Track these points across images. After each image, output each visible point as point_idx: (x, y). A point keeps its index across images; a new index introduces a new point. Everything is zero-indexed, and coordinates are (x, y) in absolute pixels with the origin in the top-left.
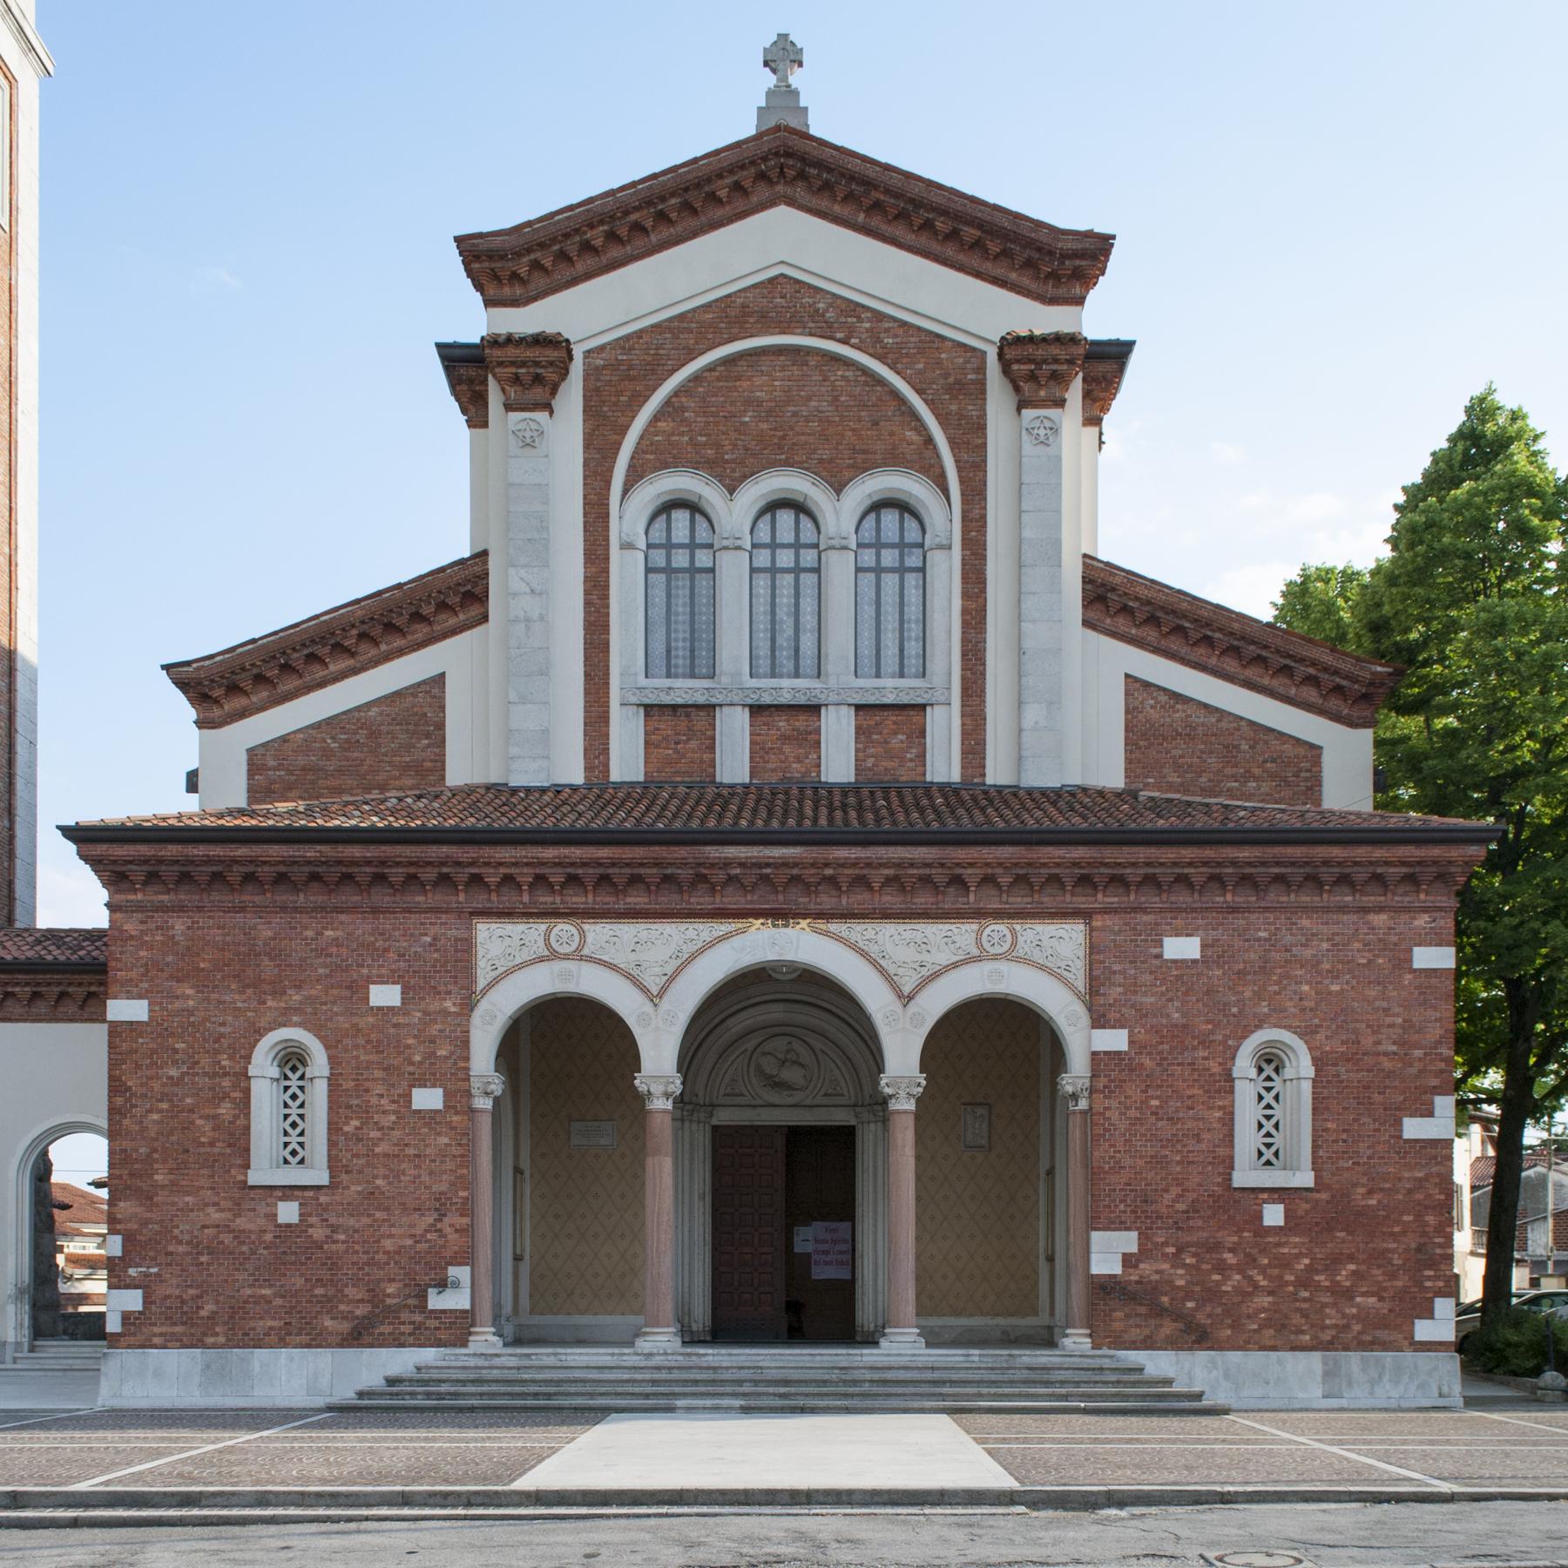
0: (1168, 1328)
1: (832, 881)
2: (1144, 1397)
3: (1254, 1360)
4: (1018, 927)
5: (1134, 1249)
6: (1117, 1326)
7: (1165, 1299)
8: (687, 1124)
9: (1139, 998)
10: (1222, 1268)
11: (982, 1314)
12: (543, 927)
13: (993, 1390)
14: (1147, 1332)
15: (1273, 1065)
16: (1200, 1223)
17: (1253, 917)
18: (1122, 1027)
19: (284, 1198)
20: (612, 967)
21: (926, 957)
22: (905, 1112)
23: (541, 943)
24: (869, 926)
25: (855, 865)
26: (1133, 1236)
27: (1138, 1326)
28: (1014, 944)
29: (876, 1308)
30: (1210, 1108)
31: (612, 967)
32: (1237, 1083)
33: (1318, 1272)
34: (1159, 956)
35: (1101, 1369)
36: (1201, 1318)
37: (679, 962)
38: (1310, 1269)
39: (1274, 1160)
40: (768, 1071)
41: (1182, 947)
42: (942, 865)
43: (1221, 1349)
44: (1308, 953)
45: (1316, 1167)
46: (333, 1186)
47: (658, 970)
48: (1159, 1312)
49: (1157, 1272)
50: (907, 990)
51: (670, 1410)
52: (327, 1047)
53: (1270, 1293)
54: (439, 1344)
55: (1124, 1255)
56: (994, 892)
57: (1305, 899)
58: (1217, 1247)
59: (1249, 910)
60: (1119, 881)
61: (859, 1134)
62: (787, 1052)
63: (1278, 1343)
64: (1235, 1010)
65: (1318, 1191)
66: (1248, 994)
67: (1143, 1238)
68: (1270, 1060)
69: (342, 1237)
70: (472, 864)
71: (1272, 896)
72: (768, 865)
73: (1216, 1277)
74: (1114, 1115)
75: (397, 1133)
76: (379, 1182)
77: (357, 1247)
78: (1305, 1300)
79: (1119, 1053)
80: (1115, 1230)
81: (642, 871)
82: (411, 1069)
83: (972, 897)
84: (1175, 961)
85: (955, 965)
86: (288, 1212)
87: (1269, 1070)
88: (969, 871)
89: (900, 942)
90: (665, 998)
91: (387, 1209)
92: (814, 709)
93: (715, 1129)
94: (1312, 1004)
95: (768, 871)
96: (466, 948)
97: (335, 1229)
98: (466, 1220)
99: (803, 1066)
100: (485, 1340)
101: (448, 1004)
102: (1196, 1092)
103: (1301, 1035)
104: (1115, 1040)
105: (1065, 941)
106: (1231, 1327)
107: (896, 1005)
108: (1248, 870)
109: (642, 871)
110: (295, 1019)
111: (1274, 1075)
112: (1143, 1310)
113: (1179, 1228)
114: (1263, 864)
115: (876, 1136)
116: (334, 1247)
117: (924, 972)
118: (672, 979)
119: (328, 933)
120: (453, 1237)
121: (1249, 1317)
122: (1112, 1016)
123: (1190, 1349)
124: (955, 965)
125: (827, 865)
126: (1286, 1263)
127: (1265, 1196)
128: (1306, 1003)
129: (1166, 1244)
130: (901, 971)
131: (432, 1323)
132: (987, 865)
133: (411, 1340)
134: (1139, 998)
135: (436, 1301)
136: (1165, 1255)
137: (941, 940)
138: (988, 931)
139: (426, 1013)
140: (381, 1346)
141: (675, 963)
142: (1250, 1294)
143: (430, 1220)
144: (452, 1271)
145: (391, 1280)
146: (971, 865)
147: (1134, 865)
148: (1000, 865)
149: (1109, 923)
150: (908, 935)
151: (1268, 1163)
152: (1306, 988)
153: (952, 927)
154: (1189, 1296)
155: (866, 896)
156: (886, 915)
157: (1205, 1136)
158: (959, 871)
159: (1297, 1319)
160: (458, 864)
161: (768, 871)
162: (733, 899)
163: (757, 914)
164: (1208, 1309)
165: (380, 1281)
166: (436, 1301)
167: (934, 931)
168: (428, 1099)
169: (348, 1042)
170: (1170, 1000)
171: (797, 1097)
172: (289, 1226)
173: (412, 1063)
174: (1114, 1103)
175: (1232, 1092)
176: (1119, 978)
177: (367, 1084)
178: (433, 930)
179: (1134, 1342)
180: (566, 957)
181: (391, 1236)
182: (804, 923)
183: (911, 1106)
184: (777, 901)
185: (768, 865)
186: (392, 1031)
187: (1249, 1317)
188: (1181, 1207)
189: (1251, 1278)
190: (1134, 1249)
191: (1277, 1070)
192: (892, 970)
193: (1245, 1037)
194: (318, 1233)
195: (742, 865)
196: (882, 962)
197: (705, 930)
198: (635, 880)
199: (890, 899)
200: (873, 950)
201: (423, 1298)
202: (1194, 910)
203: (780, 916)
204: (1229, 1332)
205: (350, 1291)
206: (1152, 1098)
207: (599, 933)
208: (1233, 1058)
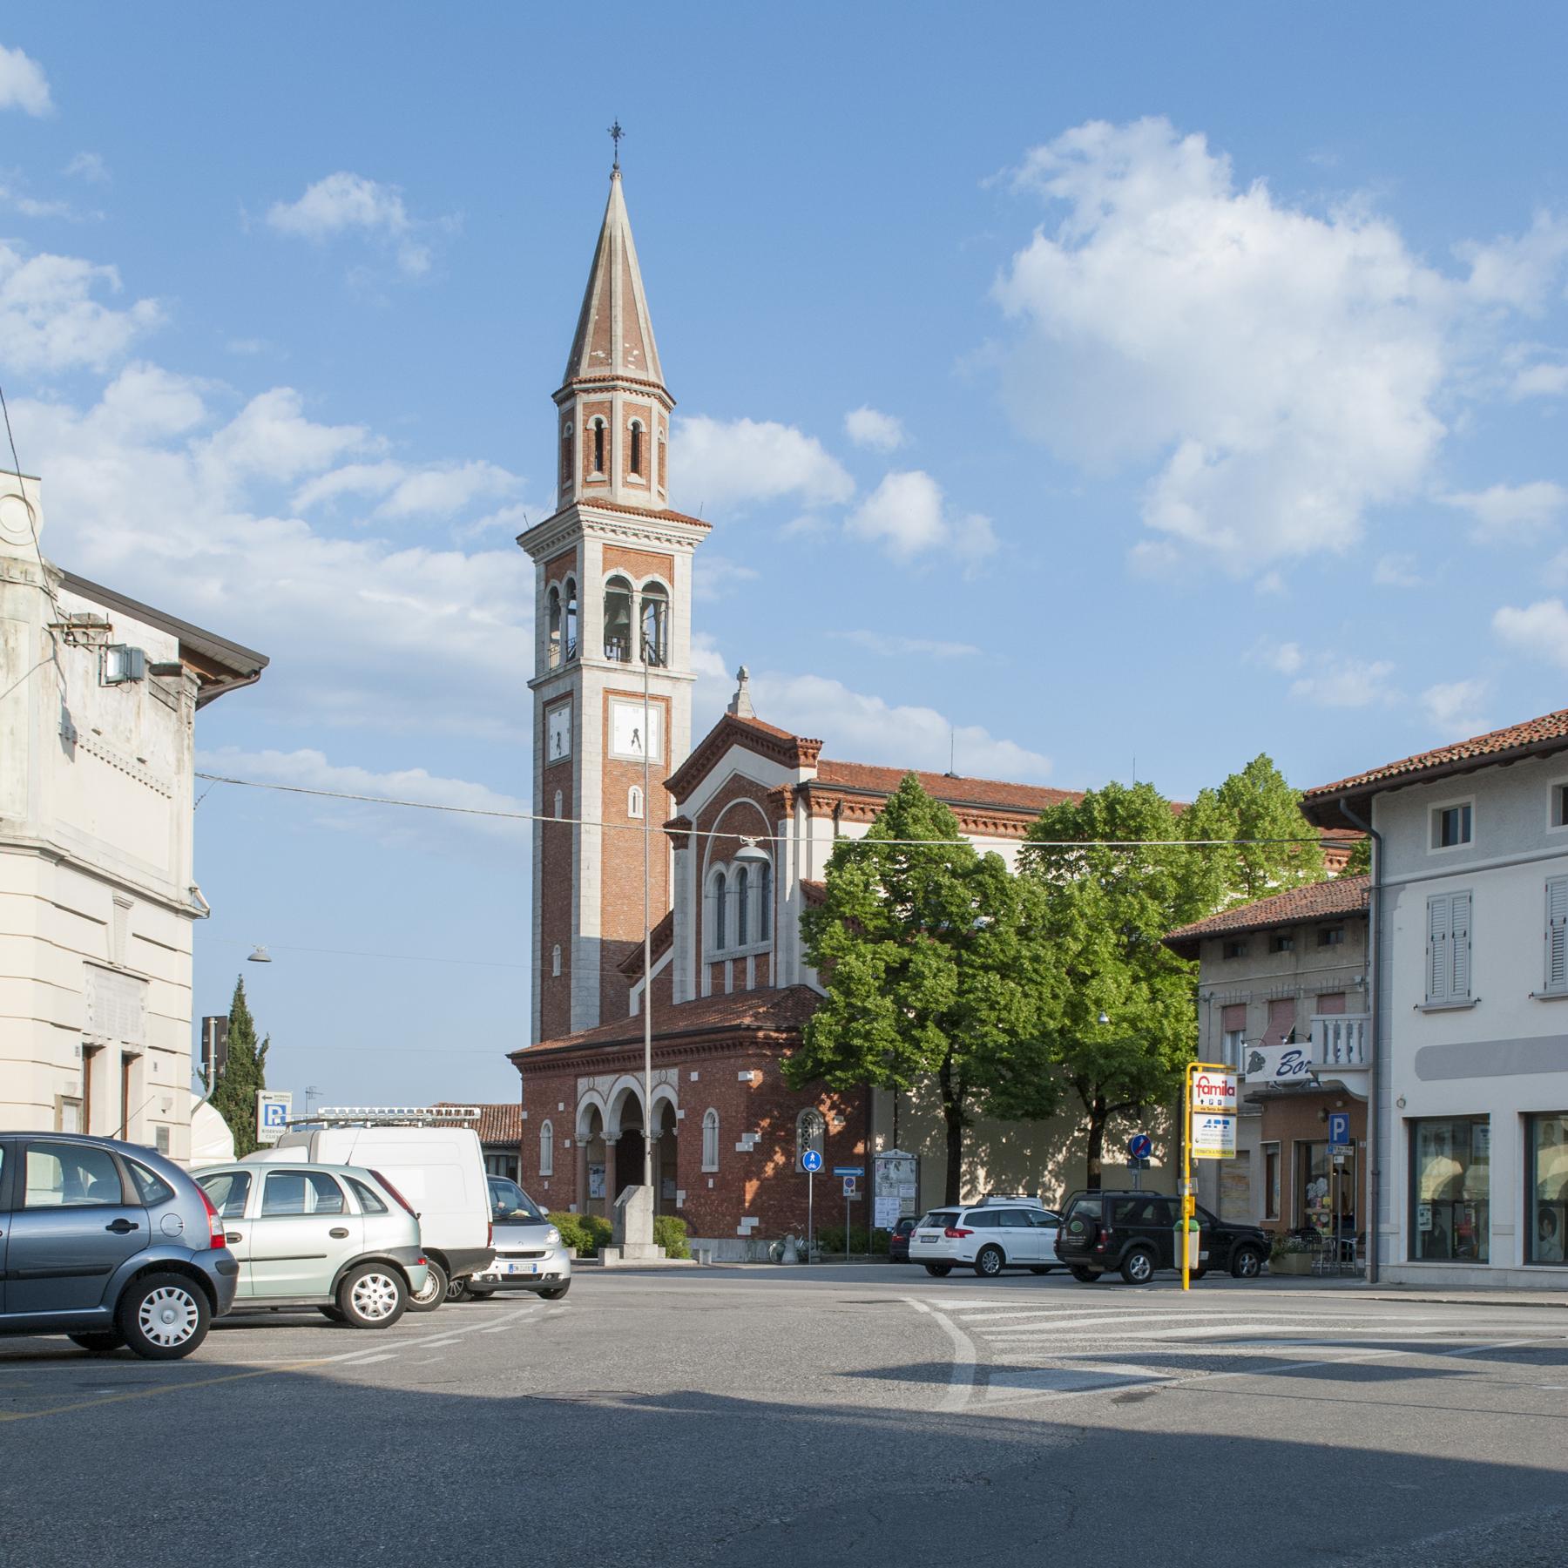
92: (744, 959)
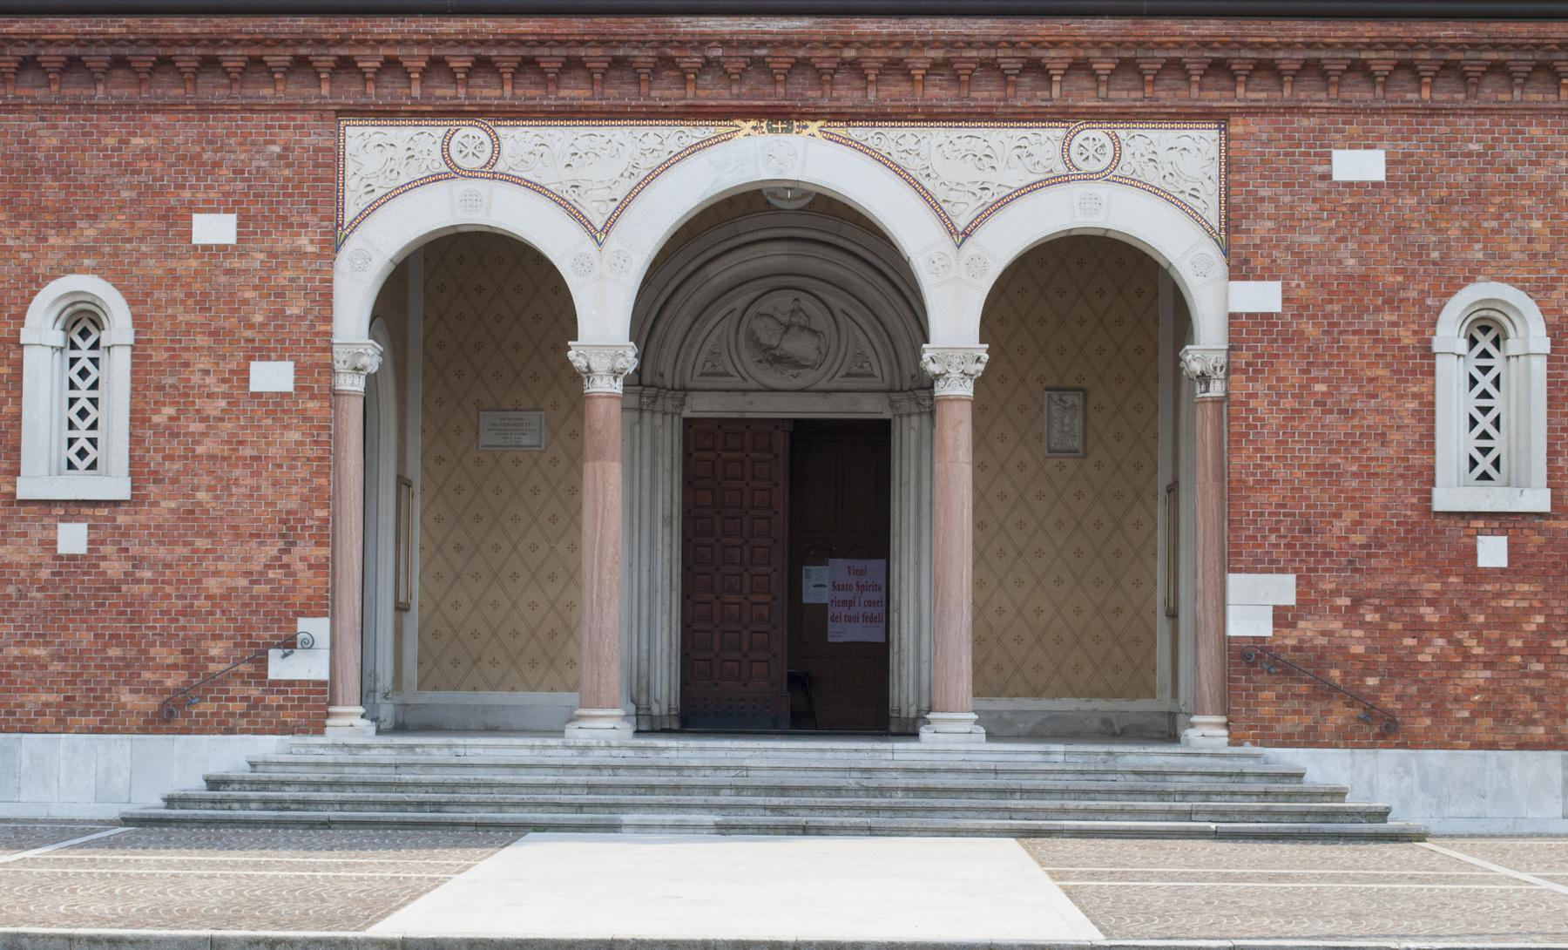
0: (1339, 715)
1: (855, 67)
2: (1303, 815)
3: (1464, 762)
4: (1122, 134)
5: (1290, 599)
6: (1265, 711)
7: (1335, 673)
8: (647, 416)
9: (1297, 237)
10: (1417, 628)
12: (441, 131)
13: (1083, 804)
14: (1309, 720)
15: (1492, 335)
16: (1386, 563)
17: (1460, 122)
18: (1273, 278)
19: (67, 518)
22: (959, 399)
23: (437, 155)
25: (887, 44)
26: (1290, 580)
27: (1298, 712)
28: (1117, 158)
30: (1400, 396)
32: (1439, 359)
33: (1556, 635)
34: (1326, 177)
35: (1242, 774)
36: (1388, 702)
38: (1546, 631)
39: (1492, 472)
41: (1359, 165)
42: (1013, 45)
43: (1416, 746)
44: (1539, 174)
45: (1554, 481)
46: (137, 500)
47: (605, 194)
48: (1327, 691)
49: (1324, 633)
51: (613, 828)
52: (132, 303)
53: (1489, 665)
54: (283, 729)
55: (1276, 608)
56: (1087, 83)
57: (1535, 97)
58: (1411, 597)
59: (1454, 112)
60: (1266, 69)
63: (1499, 738)
64: (1435, 255)
65: (1556, 518)
66: (1454, 233)
67: (1304, 583)
68: (1487, 329)
69: (148, 574)
70: (341, 42)
71: (1487, 92)
72: (762, 44)
73: (1409, 642)
74: (1262, 406)
75: (227, 426)
76: (201, 496)
77: (168, 589)
78: (1538, 675)
79: (1267, 316)
80: (1263, 571)
81: (582, 52)
82: (249, 333)
84: (1349, 184)
85: (1032, 188)
86: (72, 538)
87: (1485, 342)
88: (1053, 53)
89: (941, 149)
90: (612, 235)
91: (211, 535)
93: (688, 423)
94: (1547, 248)
95: (763, 52)
96: (331, 162)
97: (138, 562)
98: (325, 552)
99: (814, 332)
100: (349, 725)
101: (303, 241)
102: (1380, 372)
103: (1530, 292)
104: (1263, 297)
105: (1189, 154)
106: (1431, 714)
108: (1452, 55)
110: (87, 262)
111: (1492, 350)
112: (1302, 688)
113: (1355, 570)
114: (1474, 46)
116: (136, 589)
117: (988, 198)
118: (623, 206)
119: (137, 141)
120: (305, 575)
121: (1456, 700)
122: (1259, 262)
123: (1372, 746)
124: (1032, 188)
125: (847, 44)
126: (1510, 622)
127: (1480, 524)
128: (1537, 247)
129: (1336, 593)
130: (953, 196)
131: (274, 699)
132: (1078, 44)
133: (244, 723)
134: (1297, 237)
135: (280, 668)
136: (1335, 609)
137: (1007, 153)
138: (1079, 139)
139: (272, 254)
140: (200, 732)
142: (1459, 667)
143: (274, 551)
144: (305, 625)
145: (217, 637)
146: (1055, 45)
147: (1289, 46)
148: (1097, 44)
149: (1254, 128)
150: (963, 144)
151: (1485, 476)
152: (1537, 224)
153: (1028, 133)
154: (1369, 668)
155: (904, 88)
156: (932, 116)
157: (1394, 436)
158: (1038, 53)
159: (1526, 704)
160: (321, 42)
161: (763, 52)
162: (712, 92)
163: (746, 114)
164: (1398, 688)
165: (200, 637)
166: (280, 668)
167: (1000, 139)
168: (272, 376)
169: (161, 295)
170: (1343, 240)
172: (73, 557)
173: (251, 326)
174: (1260, 388)
175: (1432, 373)
176: (1268, 208)
177: (186, 356)
178: (283, 136)
179: (1290, 735)
180: (472, 174)
181: (216, 574)
182: (814, 127)
183: (967, 390)
184: (777, 95)
185: (762, 44)
186: (223, 279)
187: (1456, 700)
188: (1359, 539)
189: (1459, 643)
190: (1290, 599)
191: (1496, 342)
192: (940, 194)
193: (1450, 294)
194: (114, 568)
195: (725, 43)
198: (572, 65)
199: (938, 93)
200: (913, 166)
201: (261, 662)
202: (1376, 111)
203: (779, 115)
204: (1428, 722)
205: (158, 652)
206: (1316, 380)
207: (519, 140)
208: (1434, 324)
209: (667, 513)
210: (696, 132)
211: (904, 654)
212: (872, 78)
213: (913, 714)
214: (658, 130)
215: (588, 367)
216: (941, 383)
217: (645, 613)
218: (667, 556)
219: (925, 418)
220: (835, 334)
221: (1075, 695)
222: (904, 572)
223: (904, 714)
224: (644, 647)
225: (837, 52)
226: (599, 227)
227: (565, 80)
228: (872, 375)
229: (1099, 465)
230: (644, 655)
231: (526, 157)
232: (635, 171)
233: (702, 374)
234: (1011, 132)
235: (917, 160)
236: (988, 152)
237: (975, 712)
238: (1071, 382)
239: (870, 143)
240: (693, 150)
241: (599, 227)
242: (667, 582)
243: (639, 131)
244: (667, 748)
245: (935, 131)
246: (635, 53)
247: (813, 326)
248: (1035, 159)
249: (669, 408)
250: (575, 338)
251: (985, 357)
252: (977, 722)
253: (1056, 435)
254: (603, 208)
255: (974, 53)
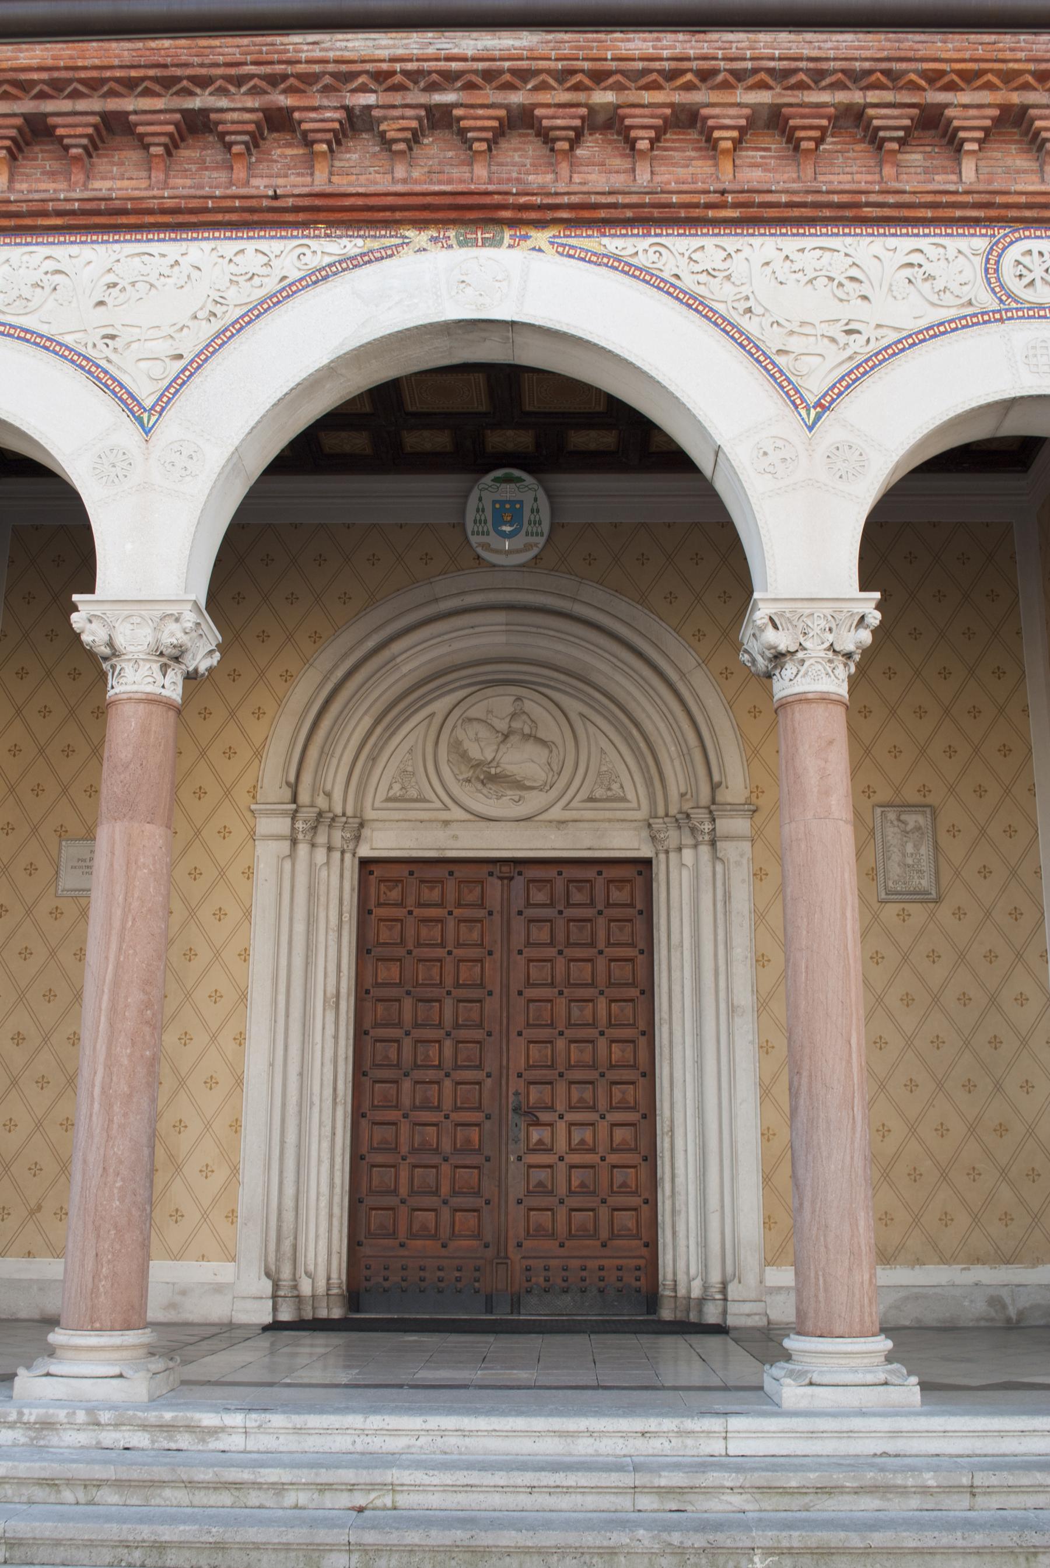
1: (611, 124)
8: (303, 849)
11: (944, 1261)
20: (47, 344)
21: (856, 310)
22: (824, 699)
24: (709, 242)
29: (704, 1244)
31: (47, 344)
37: (217, 325)
40: (474, 752)
47: (164, 348)
50: (814, 387)
61: (654, 862)
62: (513, 716)
81: (128, 104)
83: (968, 167)
85: (935, 331)
89: (789, 279)
90: (169, 414)
93: (365, 864)
95: (449, 97)
107: (788, 424)
109: (128, 104)
115: (697, 877)
118: (192, 368)
124: (935, 331)
125: (599, 77)
130: (795, 344)
132: (1008, 78)
138: (1015, 252)
141: (207, 330)
150: (809, 261)
156: (756, 215)
161: (449, 97)
171: (534, 801)
182: (541, 237)
183: (835, 682)
185: (449, 78)
192: (772, 341)
196: (744, 322)
197: (286, 254)
198: (113, 129)
199: (763, 171)
200: (721, 295)
209: (331, 989)
210: (350, 245)
211: (680, 1199)
212: (643, 145)
213: (696, 1293)
214: (264, 245)
215: (110, 644)
216: (790, 669)
217: (291, 1138)
218: (329, 1053)
219: (705, 850)
220: (570, 744)
221: (945, 1260)
222: (678, 1075)
223: (682, 1292)
224: (289, 1190)
225: (581, 97)
226: (148, 403)
227: (102, 164)
228: (624, 799)
229: (959, 913)
230: (289, 1202)
231: (27, 292)
232: (218, 310)
233: (388, 800)
234: (892, 242)
235: (728, 286)
236: (854, 272)
237: (885, 1330)
238: (911, 795)
239: (642, 260)
240: (320, 276)
241: (148, 403)
242: (328, 1092)
243: (229, 247)
244: (223, 1429)
245: (756, 241)
246: (223, 103)
247: (541, 734)
248: (939, 284)
249: (337, 842)
250: (89, 587)
251: (875, 618)
252: (890, 1358)
253: (895, 870)
254: (156, 369)
255: (825, 97)
